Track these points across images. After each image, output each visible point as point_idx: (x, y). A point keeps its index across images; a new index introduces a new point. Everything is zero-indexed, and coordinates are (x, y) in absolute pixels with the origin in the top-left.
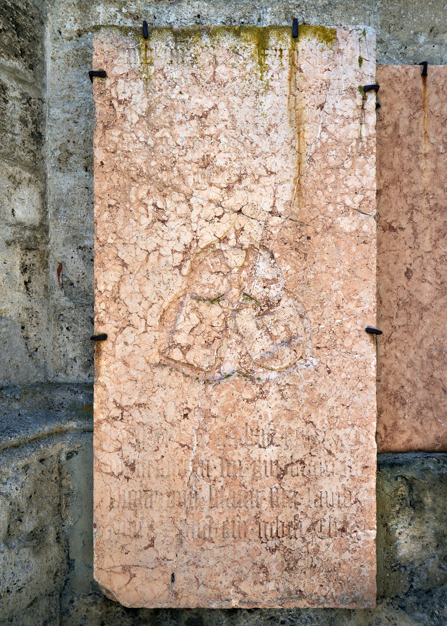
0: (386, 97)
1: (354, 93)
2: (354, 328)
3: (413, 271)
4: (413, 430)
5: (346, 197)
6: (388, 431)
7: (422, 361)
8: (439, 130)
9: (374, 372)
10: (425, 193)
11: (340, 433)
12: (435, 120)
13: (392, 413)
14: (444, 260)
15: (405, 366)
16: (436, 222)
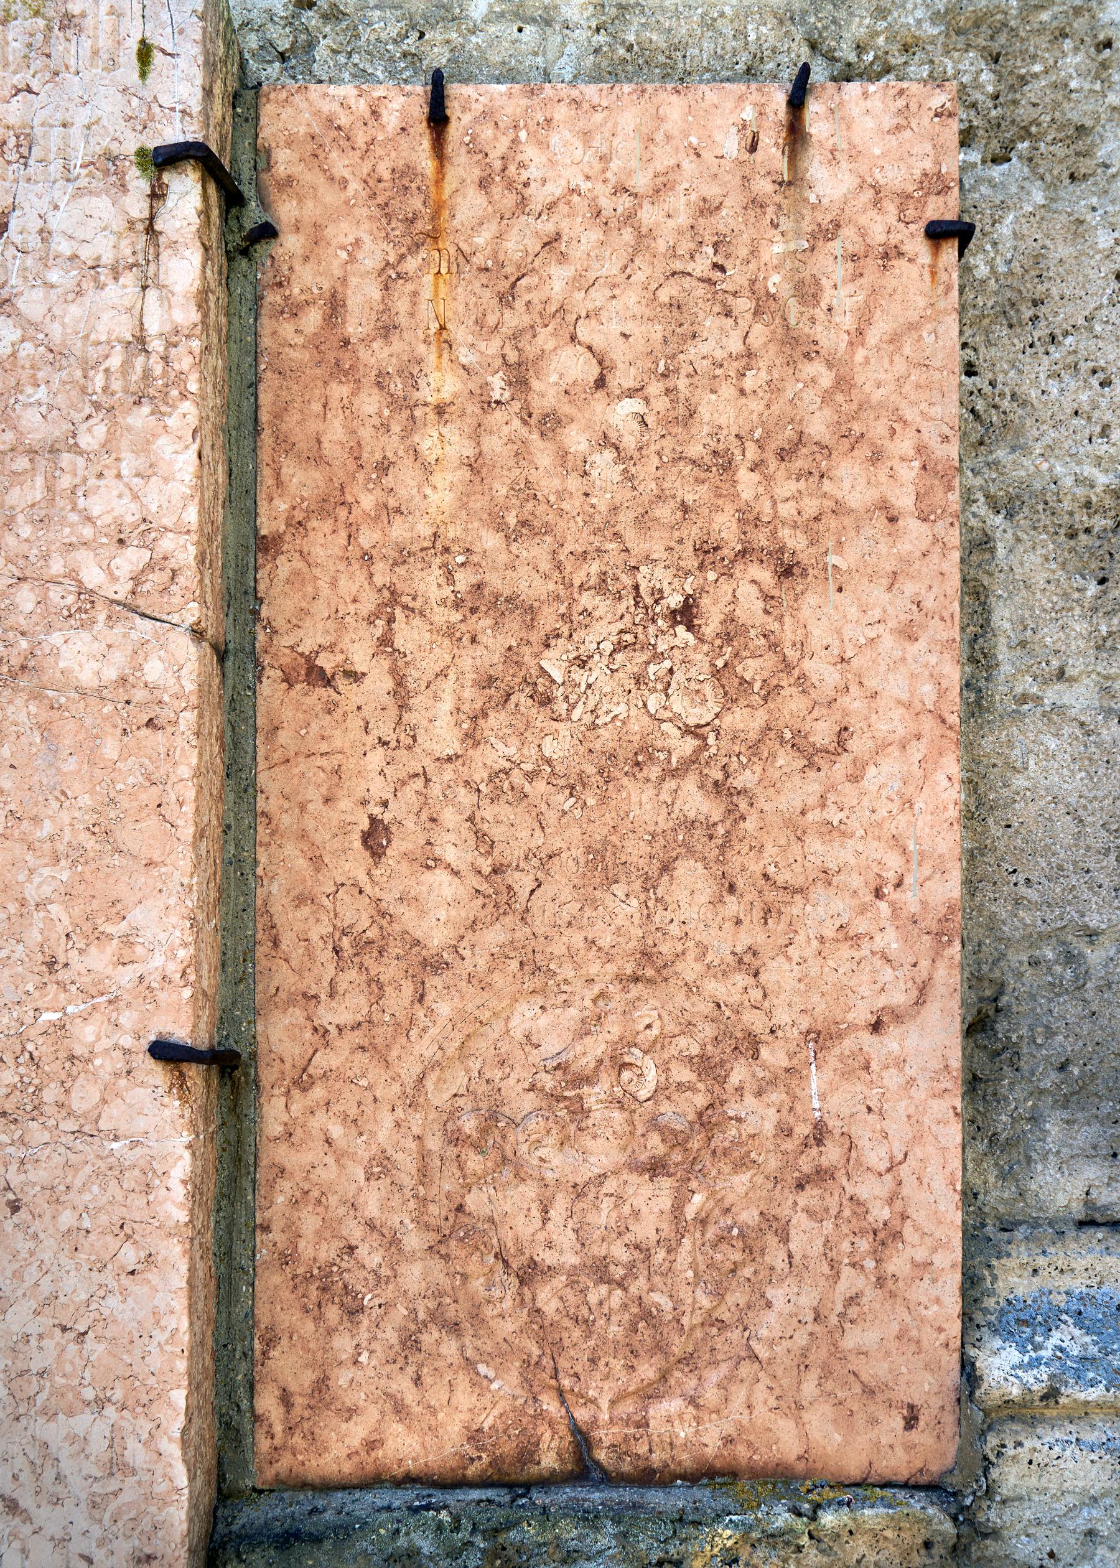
0: (300, 200)
1: (121, 175)
2: (105, 1043)
3: (394, 829)
4: (388, 1407)
5: (83, 556)
6: (297, 1411)
7: (424, 1155)
8: (491, 320)
9: (181, 1205)
10: (438, 545)
11: (54, 1432)
12: (477, 284)
13: (312, 1345)
14: (506, 786)
15: (361, 1175)
16: (479, 651)
